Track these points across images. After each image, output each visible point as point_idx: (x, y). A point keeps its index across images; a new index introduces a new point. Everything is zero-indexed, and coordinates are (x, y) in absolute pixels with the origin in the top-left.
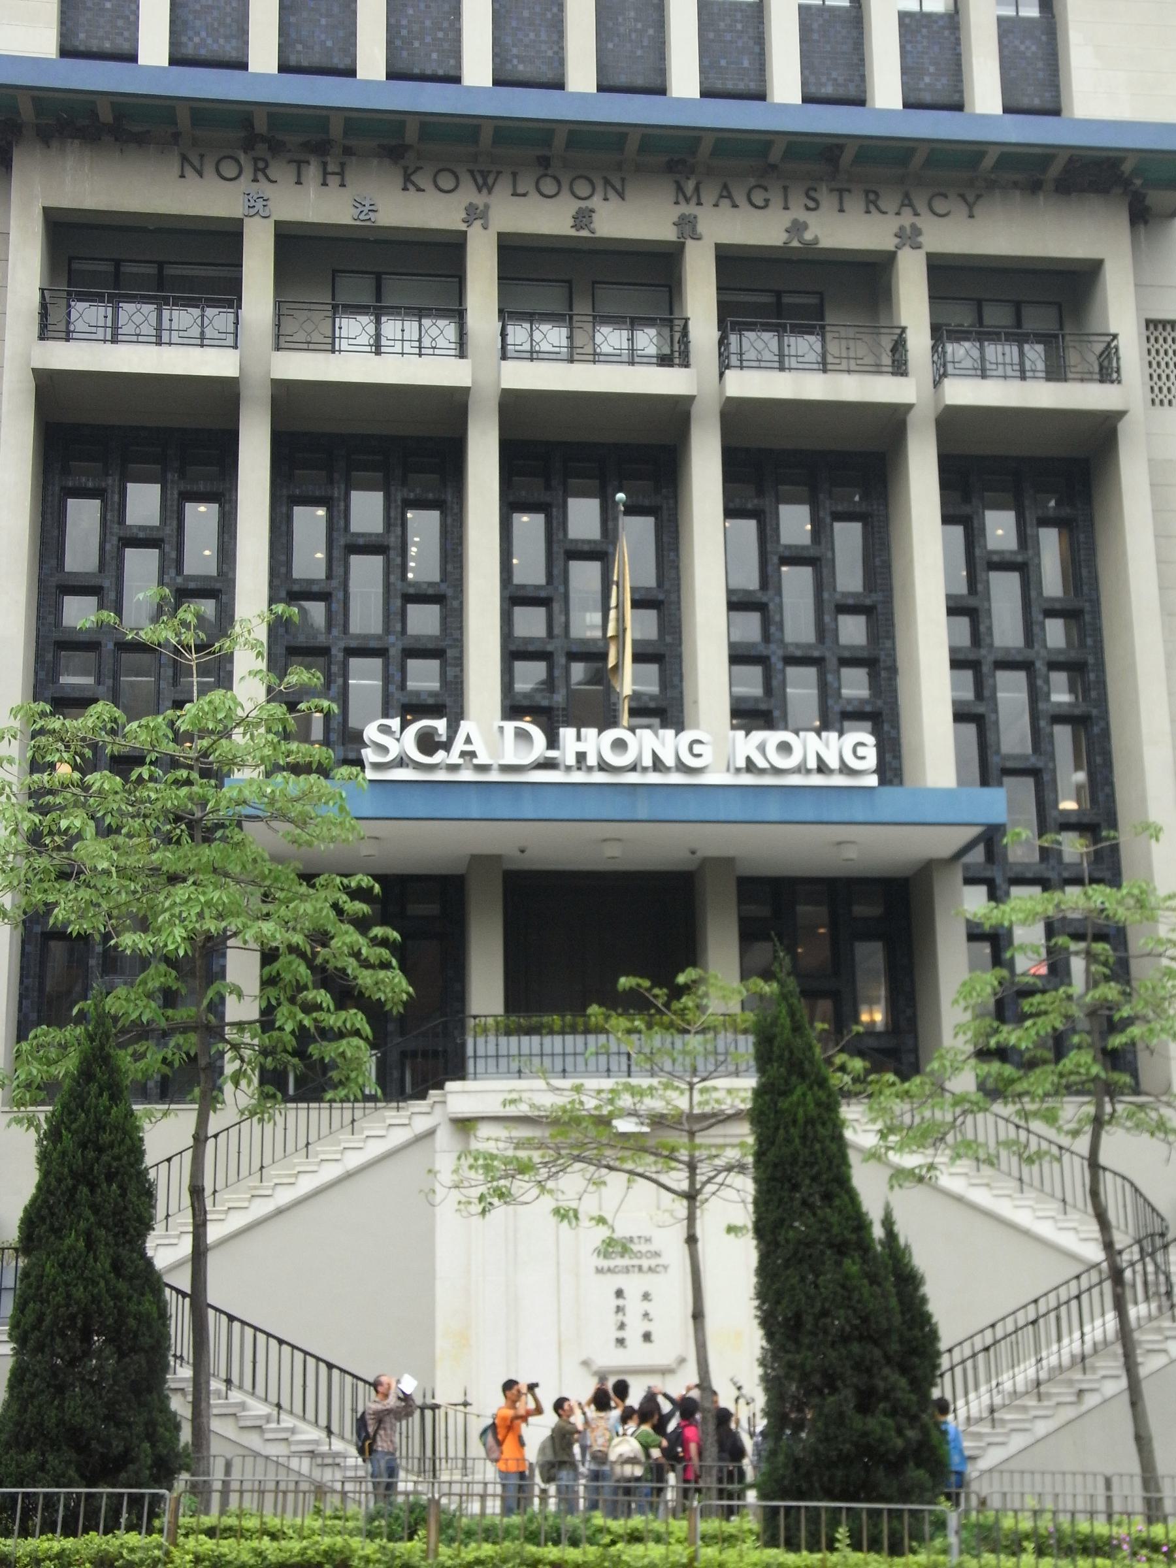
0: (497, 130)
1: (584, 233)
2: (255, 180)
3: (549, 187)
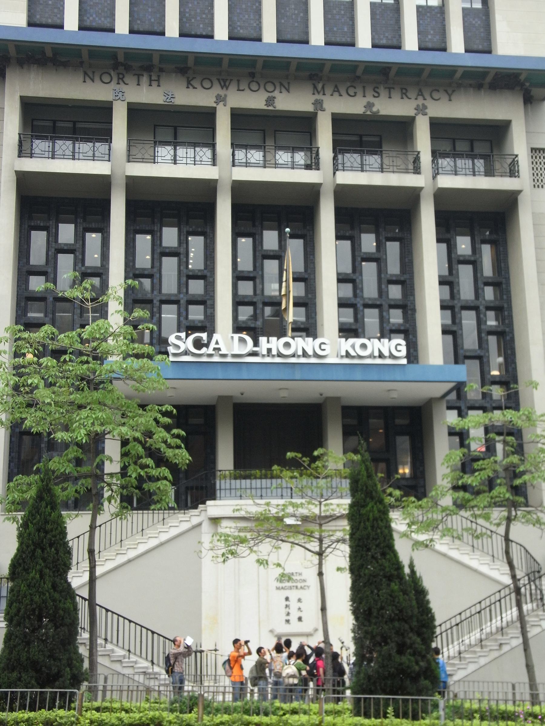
0: (230, 60)
1: (271, 108)
2: (118, 83)
3: (254, 86)
